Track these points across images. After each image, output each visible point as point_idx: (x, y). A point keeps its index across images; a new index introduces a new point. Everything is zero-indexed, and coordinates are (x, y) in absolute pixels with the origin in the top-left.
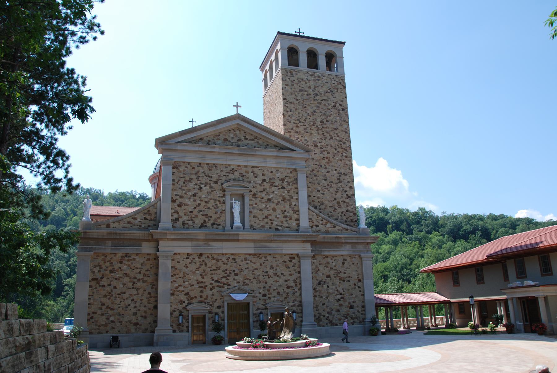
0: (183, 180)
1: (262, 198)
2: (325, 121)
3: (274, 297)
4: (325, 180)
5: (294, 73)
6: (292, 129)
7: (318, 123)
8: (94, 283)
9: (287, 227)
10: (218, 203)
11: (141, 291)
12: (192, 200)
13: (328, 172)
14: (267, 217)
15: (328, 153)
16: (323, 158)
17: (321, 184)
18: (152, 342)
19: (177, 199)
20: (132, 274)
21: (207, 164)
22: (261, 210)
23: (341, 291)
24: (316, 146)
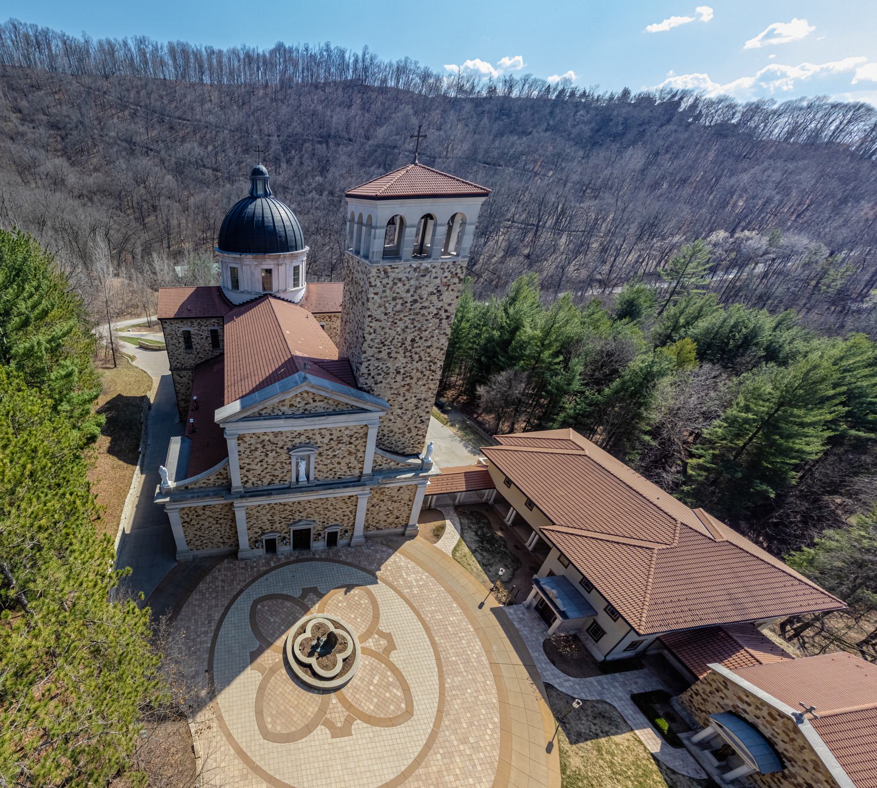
0: (249, 450)
2: (417, 339)
5: (389, 270)
7: (408, 343)
8: (185, 524)
11: (224, 525)
13: (406, 400)
15: (412, 378)
20: (215, 516)
24: (399, 372)
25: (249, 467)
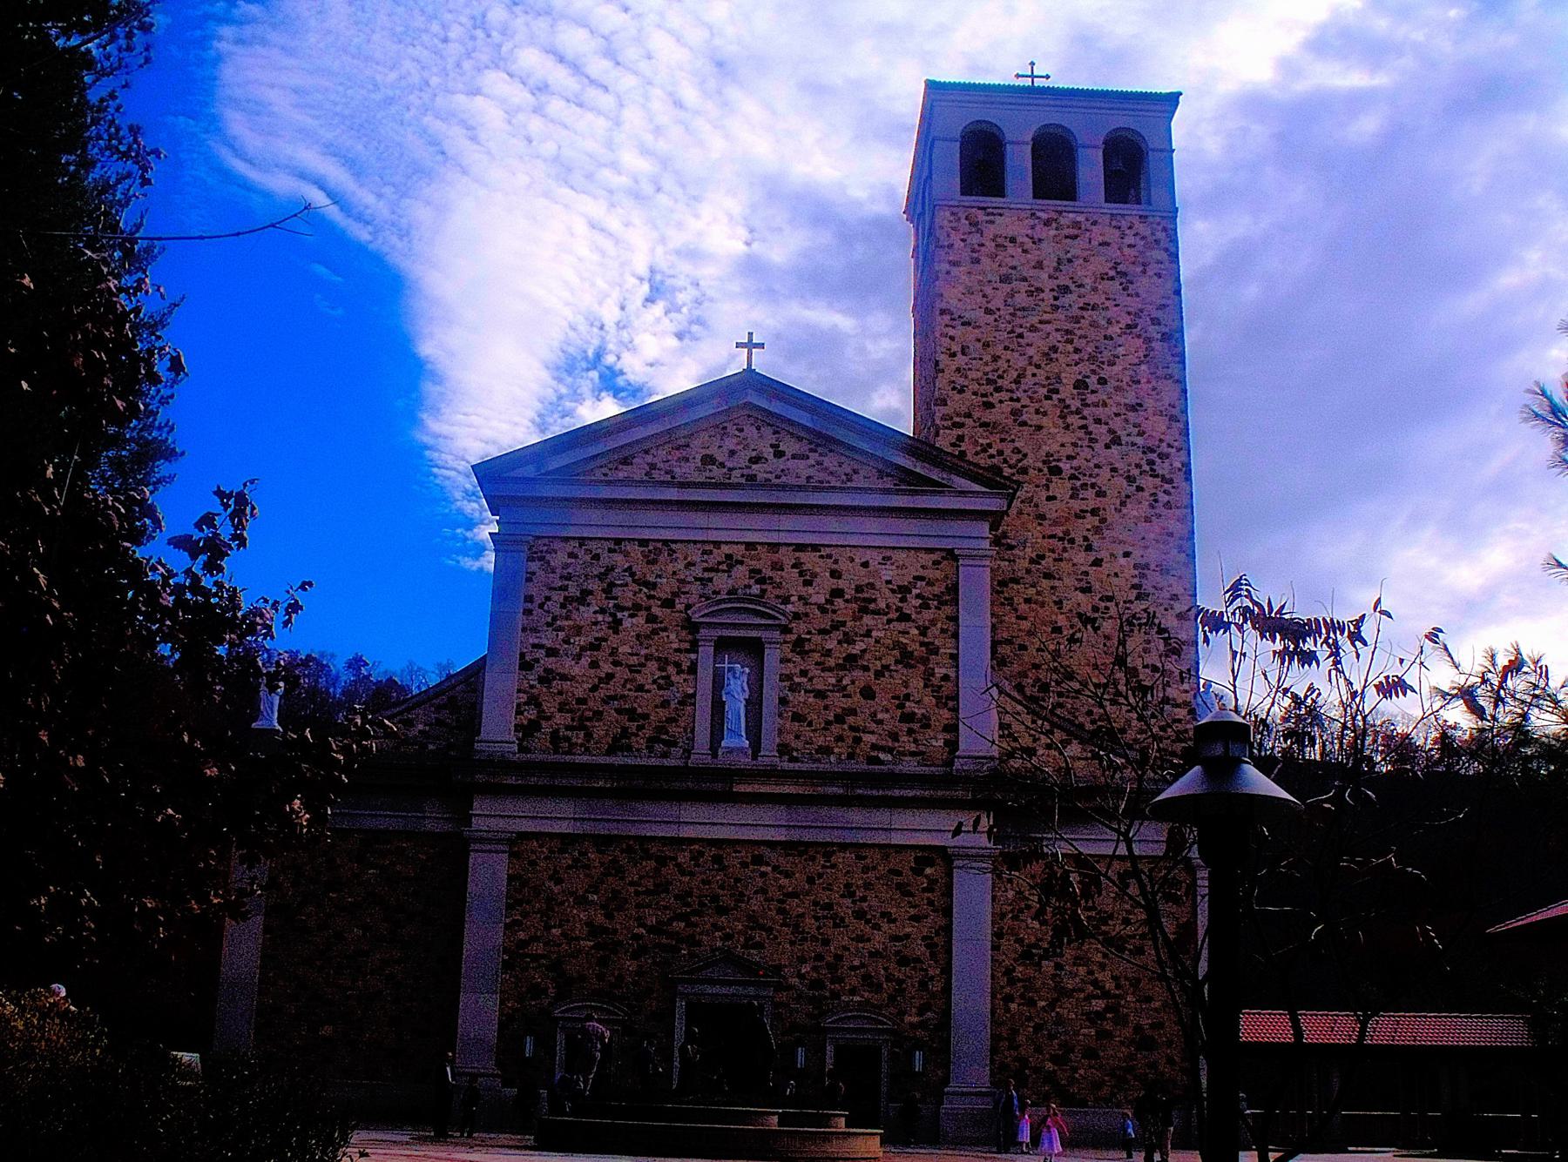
0: (558, 597)
1: (828, 653)
2: (1092, 381)
3: (853, 992)
4: (1086, 590)
6: (969, 415)
7: (1067, 391)
9: (913, 754)
10: (671, 670)
12: (585, 661)
14: (839, 719)
15: (1101, 494)
16: (1080, 515)
17: (1067, 605)
18: (439, 1116)
19: (537, 661)
21: (643, 543)
22: (820, 694)
23: (1110, 985)
24: (1056, 471)
25: (550, 662)
